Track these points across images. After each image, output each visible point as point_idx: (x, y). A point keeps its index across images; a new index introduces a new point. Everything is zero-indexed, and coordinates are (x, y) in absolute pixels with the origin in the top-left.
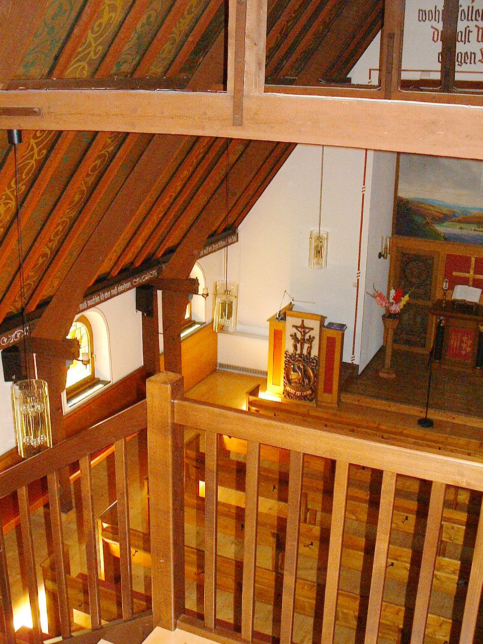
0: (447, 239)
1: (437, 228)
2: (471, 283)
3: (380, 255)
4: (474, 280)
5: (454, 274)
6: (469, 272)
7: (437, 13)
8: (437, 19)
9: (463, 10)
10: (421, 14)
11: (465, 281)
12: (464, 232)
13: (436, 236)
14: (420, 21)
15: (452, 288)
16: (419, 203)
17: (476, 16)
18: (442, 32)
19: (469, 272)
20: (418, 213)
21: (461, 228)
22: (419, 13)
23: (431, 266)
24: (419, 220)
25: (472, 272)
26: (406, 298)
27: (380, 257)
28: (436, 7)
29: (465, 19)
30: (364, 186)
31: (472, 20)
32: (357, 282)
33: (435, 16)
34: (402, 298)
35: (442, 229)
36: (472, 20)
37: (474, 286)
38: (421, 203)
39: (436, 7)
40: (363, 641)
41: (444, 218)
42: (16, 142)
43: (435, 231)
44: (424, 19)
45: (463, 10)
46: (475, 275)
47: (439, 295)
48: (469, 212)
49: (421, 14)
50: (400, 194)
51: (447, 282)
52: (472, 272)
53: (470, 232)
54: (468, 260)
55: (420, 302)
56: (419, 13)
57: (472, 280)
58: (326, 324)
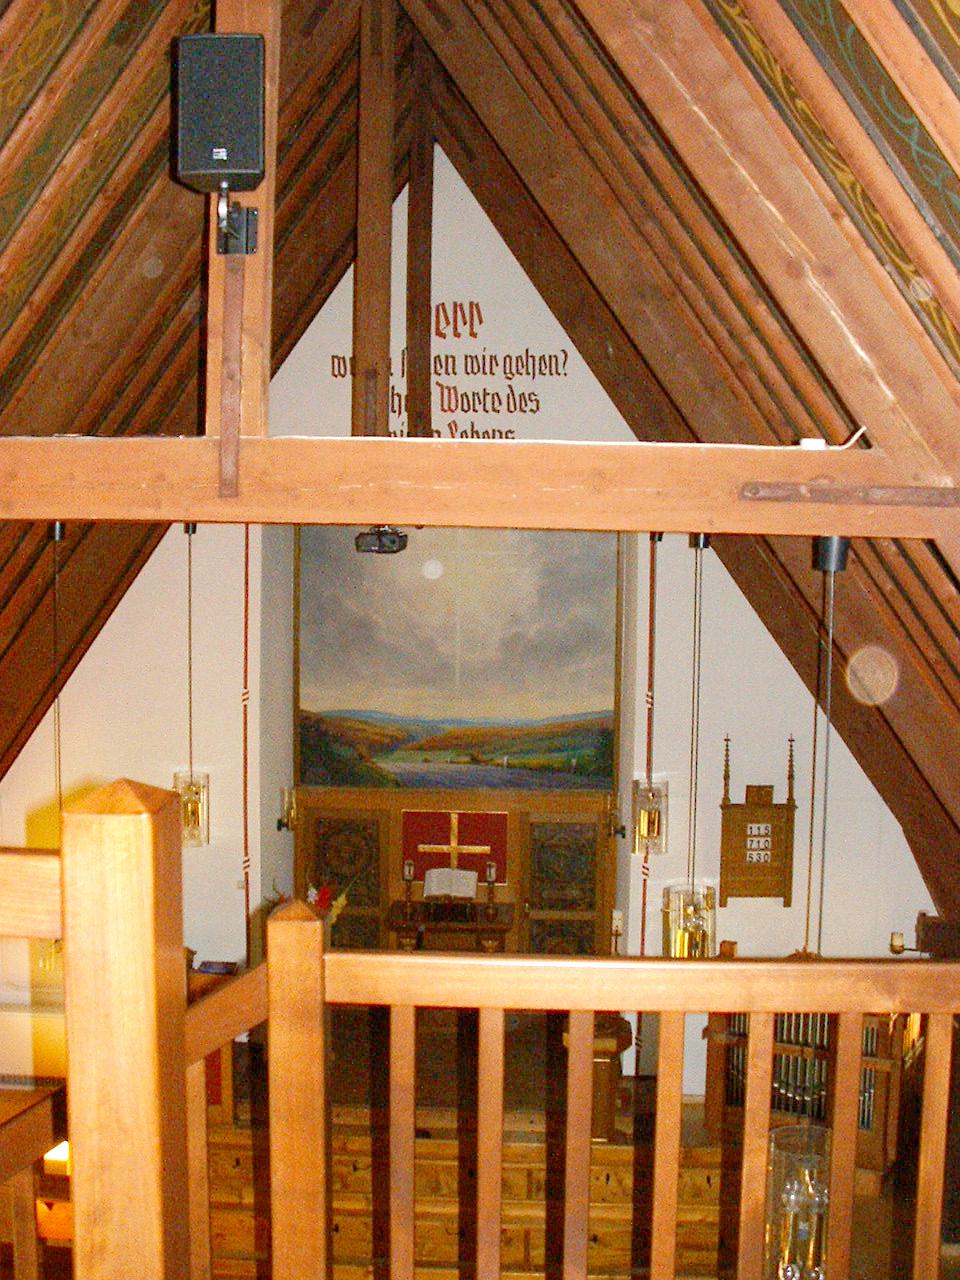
0: (401, 783)
1: (379, 764)
2: (454, 862)
3: (281, 825)
4: (462, 857)
5: (422, 848)
6: (448, 843)
7: (530, 360)
8: (530, 370)
9: (439, 356)
10: (469, 364)
11: (442, 861)
12: (432, 767)
13: (378, 780)
14: (336, 376)
15: (420, 876)
16: (340, 719)
17: (435, 367)
18: (407, 396)
19: (448, 843)
20: (341, 738)
21: (426, 761)
22: (333, 363)
23: (374, 839)
24: (346, 752)
25: (454, 843)
26: (341, 901)
27: (279, 829)
28: (527, 350)
29: (479, 371)
30: (245, 691)
31: (551, 374)
32: (243, 879)
33: (534, 365)
34: (334, 903)
35: (389, 765)
36: (551, 374)
37: (461, 866)
38: (344, 720)
39: (527, 350)
40: (561, 1275)
41: (391, 744)
42: (57, 538)
43: (379, 771)
44: (342, 372)
45: (439, 356)
46: (461, 847)
47: (396, 893)
48: (438, 729)
49: (469, 364)
50: (304, 705)
51: (410, 865)
52: (454, 843)
53: (441, 766)
54: (446, 818)
55: (366, 911)
56: (333, 363)
57: (456, 856)
58: (196, 965)
